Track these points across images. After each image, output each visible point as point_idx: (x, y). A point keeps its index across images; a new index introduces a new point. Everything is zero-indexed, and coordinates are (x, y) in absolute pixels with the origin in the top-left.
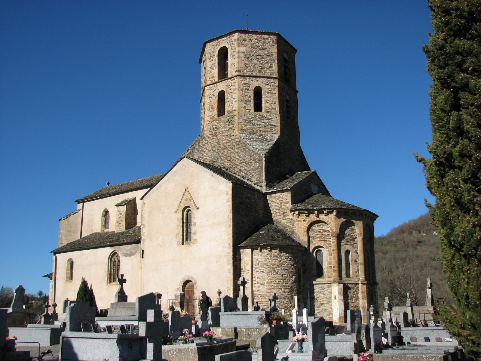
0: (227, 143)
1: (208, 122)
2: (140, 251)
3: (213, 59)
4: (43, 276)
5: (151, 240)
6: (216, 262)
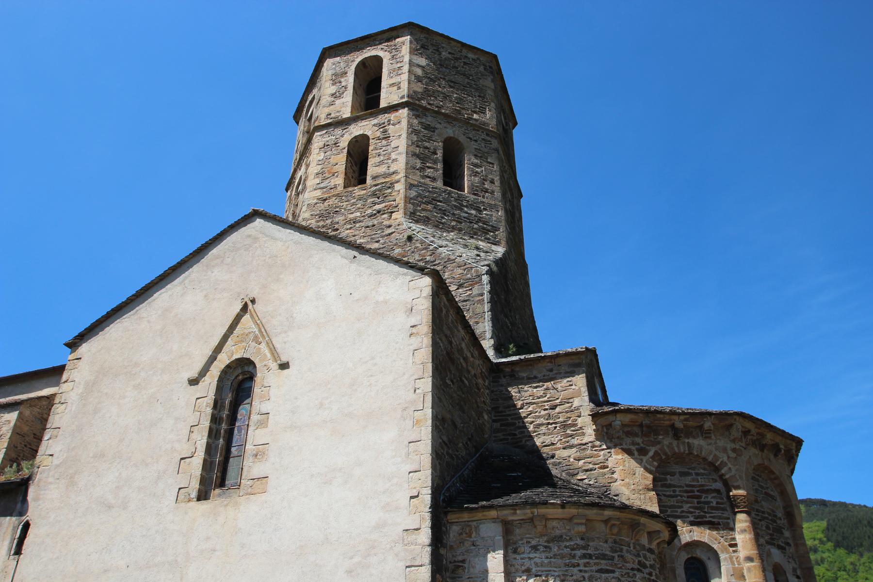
1: (315, 201)
3: (342, 80)
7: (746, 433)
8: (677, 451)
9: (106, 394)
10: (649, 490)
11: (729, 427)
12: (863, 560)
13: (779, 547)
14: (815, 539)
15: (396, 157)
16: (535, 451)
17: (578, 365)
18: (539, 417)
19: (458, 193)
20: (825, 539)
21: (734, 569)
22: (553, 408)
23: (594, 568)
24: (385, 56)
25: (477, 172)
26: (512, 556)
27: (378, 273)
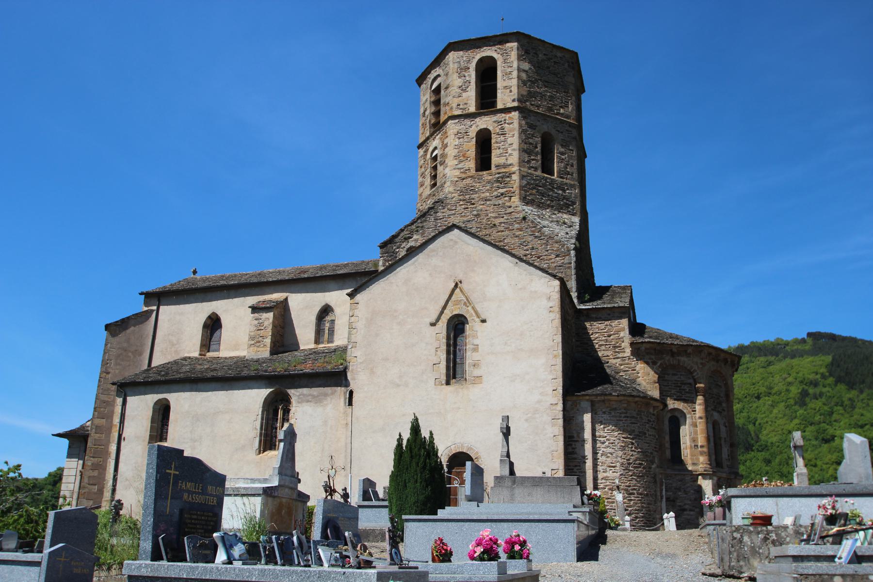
0: (496, 217)
1: (456, 179)
3: (466, 74)
4: (53, 435)
5: (372, 372)
6: (526, 420)
7: (710, 354)
8: (672, 363)
9: (381, 326)
10: (655, 383)
11: (701, 352)
12: (862, 397)
13: (718, 412)
14: (817, 373)
15: (512, 152)
16: (598, 359)
17: (624, 313)
18: (601, 340)
19: (551, 179)
20: (827, 374)
21: (692, 422)
22: (609, 336)
23: (629, 422)
24: (498, 59)
25: (563, 159)
26: (594, 415)
27: (531, 274)
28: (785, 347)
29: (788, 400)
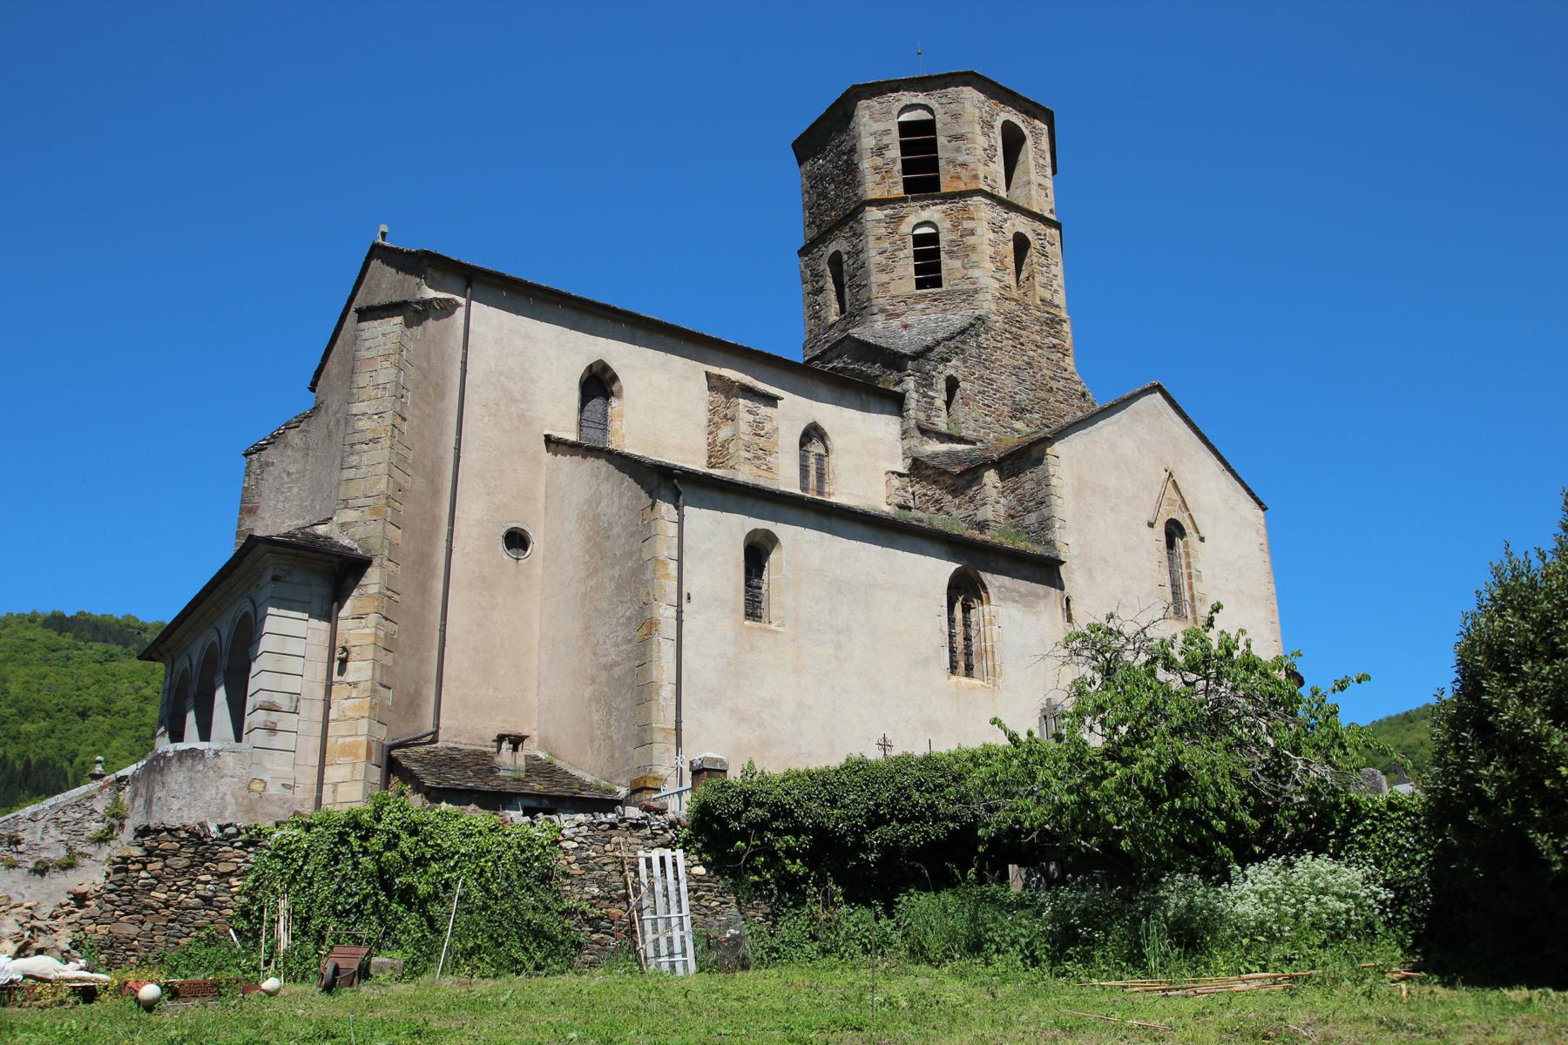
2: (1062, 600)
28: (139, 633)
29: (141, 728)
